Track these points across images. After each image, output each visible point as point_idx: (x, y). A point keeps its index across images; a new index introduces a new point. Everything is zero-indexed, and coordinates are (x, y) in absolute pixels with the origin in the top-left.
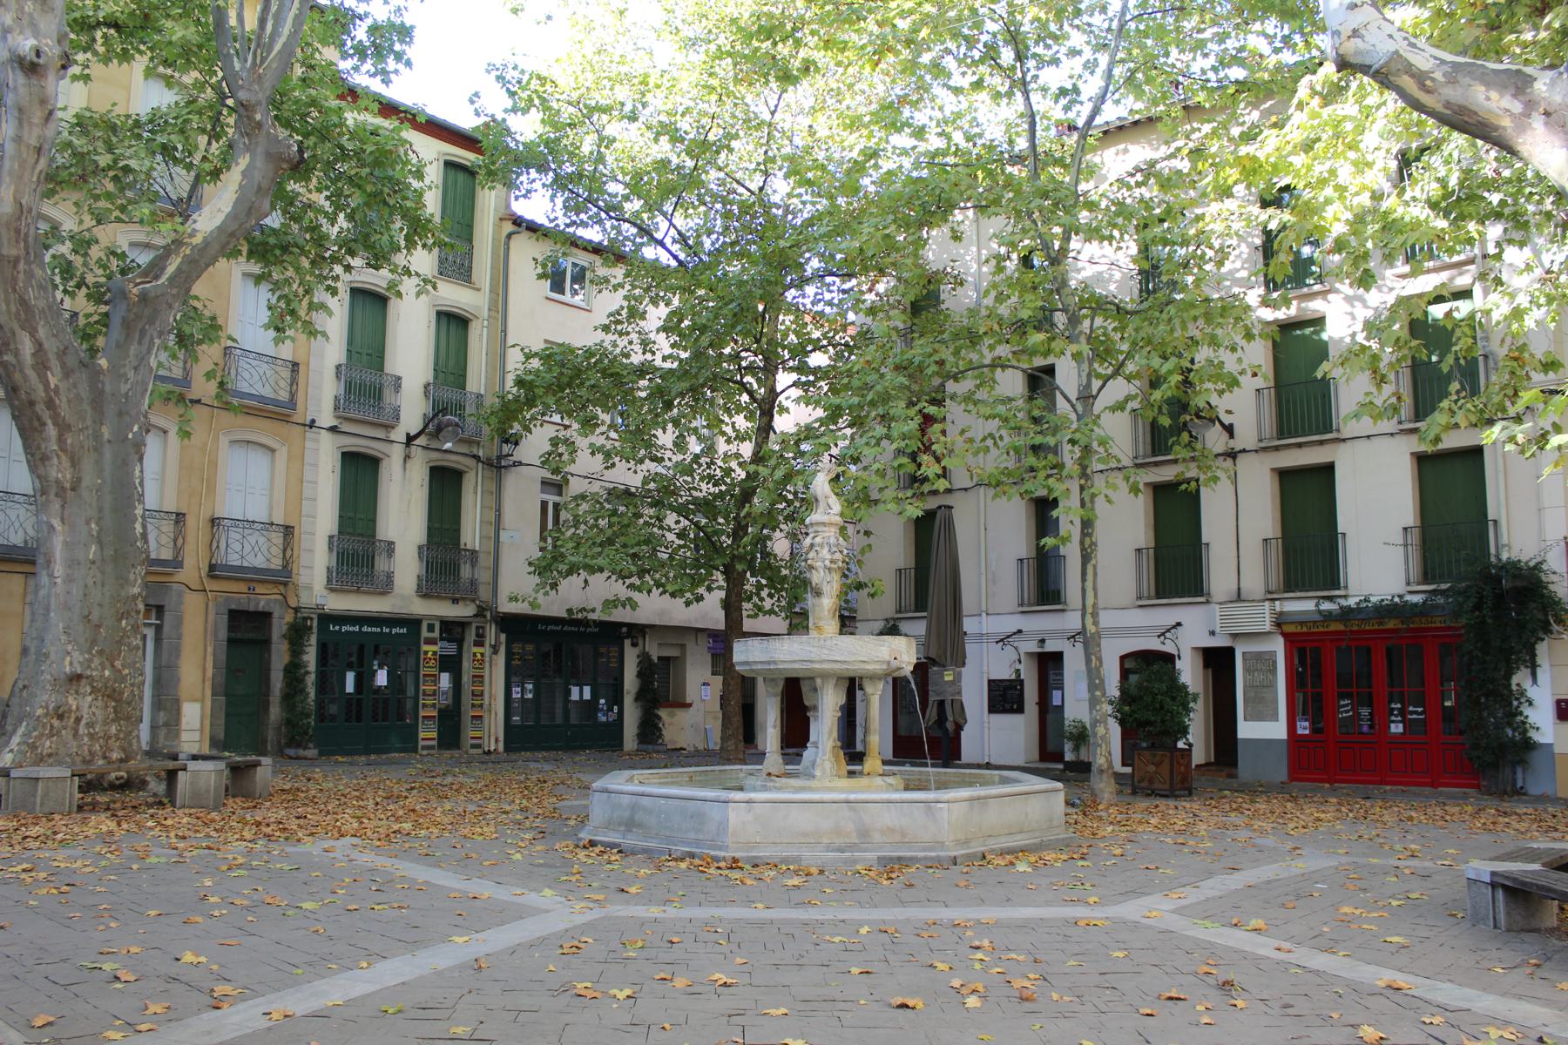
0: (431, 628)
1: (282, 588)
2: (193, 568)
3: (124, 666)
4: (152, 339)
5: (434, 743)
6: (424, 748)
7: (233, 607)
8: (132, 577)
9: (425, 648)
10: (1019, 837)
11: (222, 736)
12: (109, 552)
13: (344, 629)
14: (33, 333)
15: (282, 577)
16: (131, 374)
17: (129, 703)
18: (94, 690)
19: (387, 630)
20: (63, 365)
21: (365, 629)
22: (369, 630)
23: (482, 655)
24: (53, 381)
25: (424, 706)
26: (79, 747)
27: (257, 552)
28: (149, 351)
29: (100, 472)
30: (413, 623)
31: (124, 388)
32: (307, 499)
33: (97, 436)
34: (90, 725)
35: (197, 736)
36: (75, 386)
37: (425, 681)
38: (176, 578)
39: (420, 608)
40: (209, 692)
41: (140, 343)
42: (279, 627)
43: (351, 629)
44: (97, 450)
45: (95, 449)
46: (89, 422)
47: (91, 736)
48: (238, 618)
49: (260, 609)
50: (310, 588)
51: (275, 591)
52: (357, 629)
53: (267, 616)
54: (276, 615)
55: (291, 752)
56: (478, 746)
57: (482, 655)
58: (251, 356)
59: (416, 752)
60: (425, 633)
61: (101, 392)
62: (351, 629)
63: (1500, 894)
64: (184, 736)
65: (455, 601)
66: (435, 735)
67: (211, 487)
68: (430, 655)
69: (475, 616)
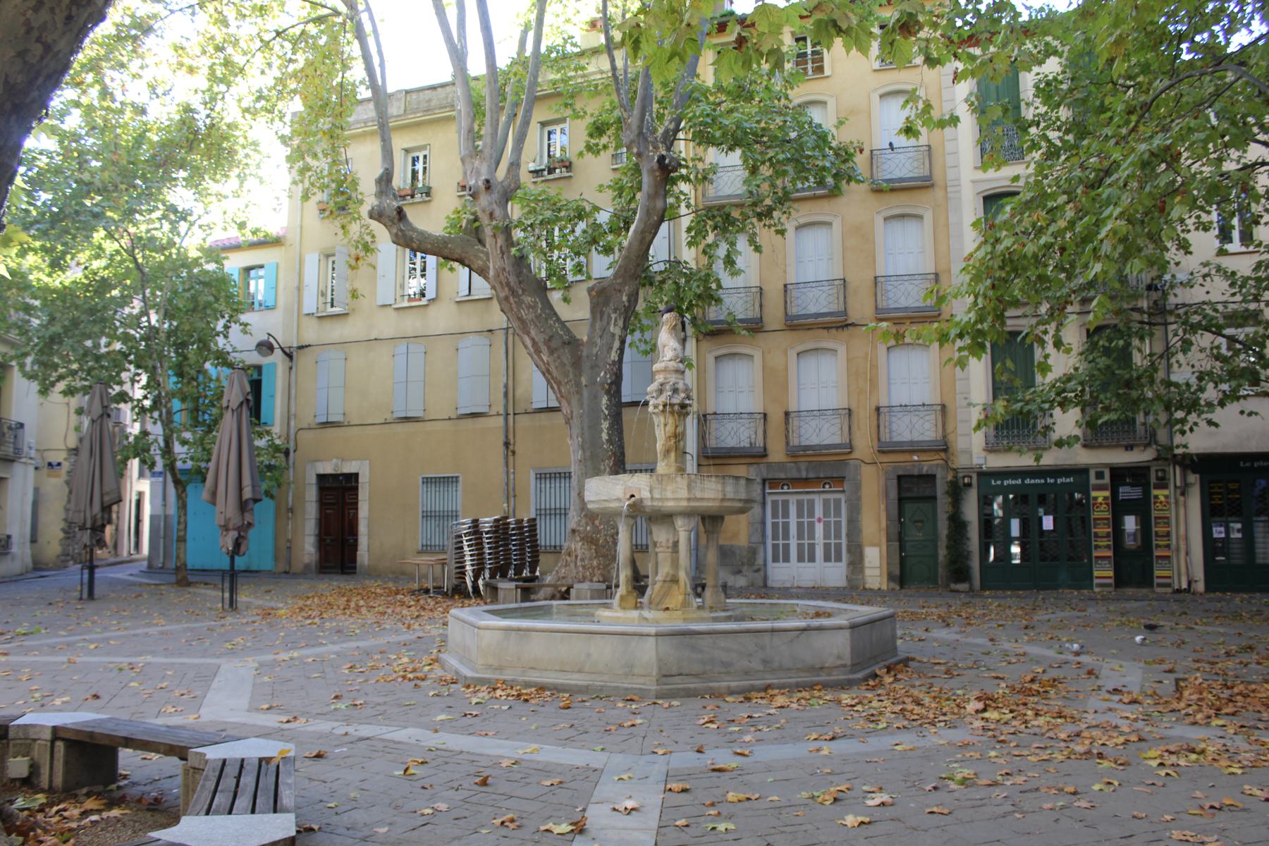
0: (1100, 475)
1: (943, 455)
2: (864, 445)
3: (600, 524)
4: (609, 317)
5: (1111, 581)
6: (1159, 585)
7: (901, 473)
8: (602, 467)
9: (1094, 494)
10: (576, 676)
11: (897, 572)
12: (588, 454)
13: (1006, 483)
14: (528, 333)
15: (943, 447)
16: (598, 341)
17: (604, 547)
18: (582, 539)
19: (1049, 480)
20: (549, 347)
21: (1028, 481)
22: (1033, 481)
23: (1166, 497)
24: (545, 358)
25: (1158, 546)
26: (577, 573)
27: (924, 429)
28: (608, 323)
29: (581, 406)
30: (1081, 472)
31: (595, 350)
32: (960, 380)
33: (578, 384)
34: (582, 560)
35: (877, 572)
36: (559, 358)
37: (1156, 523)
38: (853, 456)
39: (1082, 457)
40: (884, 540)
41: (601, 320)
42: (941, 488)
43: (1014, 482)
44: (579, 392)
45: (577, 392)
46: (571, 376)
47: (584, 567)
48: (904, 481)
49: (924, 472)
50: (969, 452)
51: (937, 457)
52: (1019, 482)
53: (932, 478)
54: (938, 476)
55: (953, 586)
56: (1168, 585)
57: (1166, 497)
58: (892, 279)
59: (1092, 589)
60: (1093, 480)
61: (580, 357)
62: (1014, 482)
63: (60, 745)
64: (868, 572)
65: (1129, 448)
66: (1111, 574)
67: (874, 383)
68: (1100, 500)
69: (1154, 460)
